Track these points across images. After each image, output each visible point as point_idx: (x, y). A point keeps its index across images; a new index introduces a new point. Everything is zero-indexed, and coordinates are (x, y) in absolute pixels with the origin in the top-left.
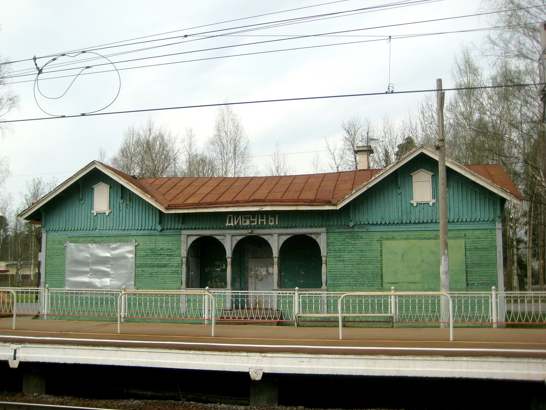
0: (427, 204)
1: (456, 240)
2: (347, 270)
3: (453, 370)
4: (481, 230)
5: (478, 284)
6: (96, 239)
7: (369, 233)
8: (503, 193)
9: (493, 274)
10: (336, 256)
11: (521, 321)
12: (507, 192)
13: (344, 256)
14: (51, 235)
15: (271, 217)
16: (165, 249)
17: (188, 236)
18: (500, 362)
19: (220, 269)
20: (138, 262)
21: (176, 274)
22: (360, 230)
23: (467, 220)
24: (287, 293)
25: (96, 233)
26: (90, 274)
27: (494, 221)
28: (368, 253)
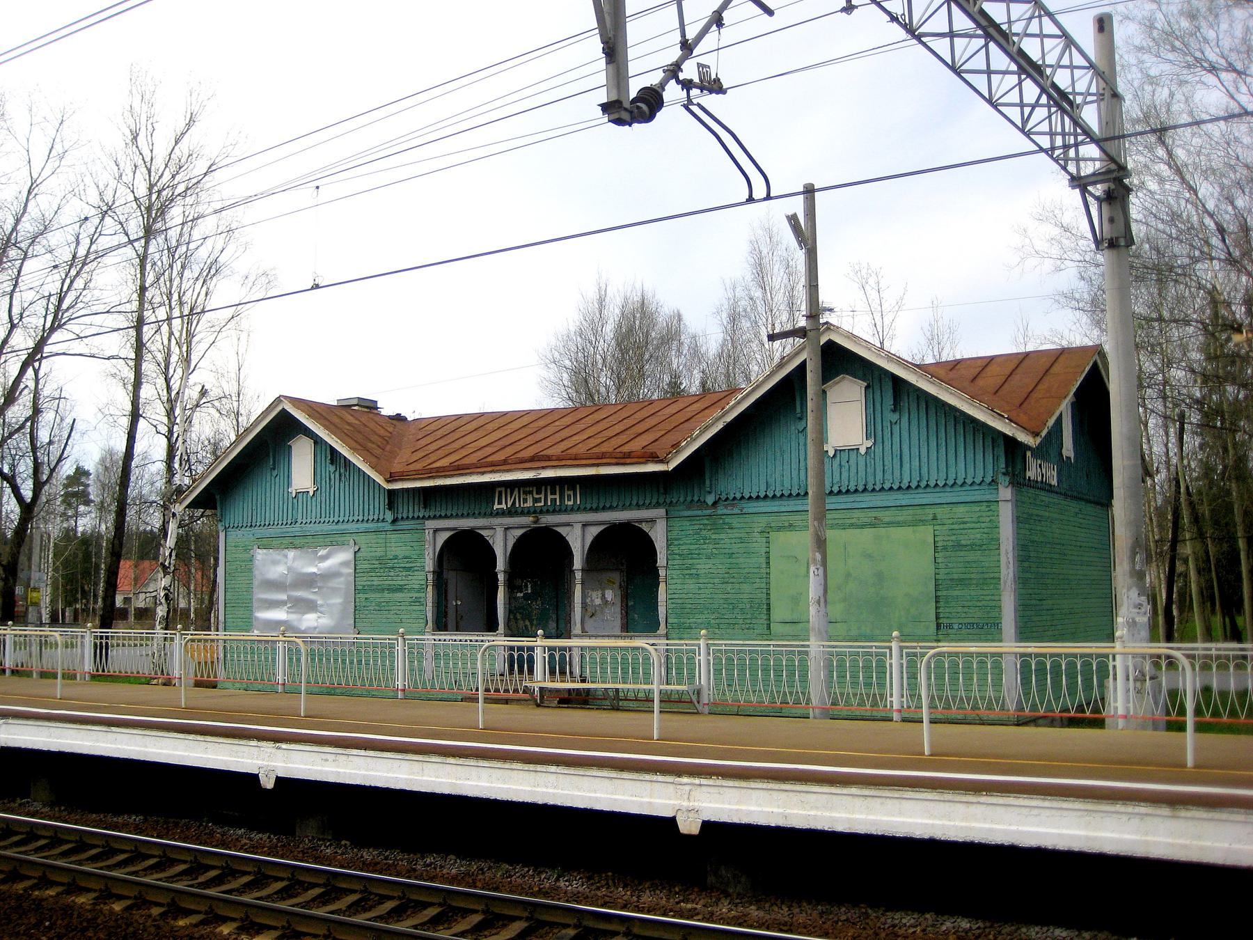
0: (855, 451)
1: (915, 528)
2: (704, 596)
3: (534, 789)
4: (967, 505)
5: (960, 626)
6: (297, 541)
7: (745, 516)
8: (997, 420)
9: (991, 604)
10: (684, 567)
11: (1083, 711)
12: (1003, 416)
13: (698, 566)
14: (233, 534)
15: (568, 490)
16: (400, 557)
17: (436, 531)
18: (608, 778)
19: (522, 595)
20: (360, 583)
21: (417, 604)
22: (729, 512)
23: (902, 485)
24: (525, 642)
25: (296, 529)
26: (289, 605)
27: (994, 481)
28: (741, 560)
